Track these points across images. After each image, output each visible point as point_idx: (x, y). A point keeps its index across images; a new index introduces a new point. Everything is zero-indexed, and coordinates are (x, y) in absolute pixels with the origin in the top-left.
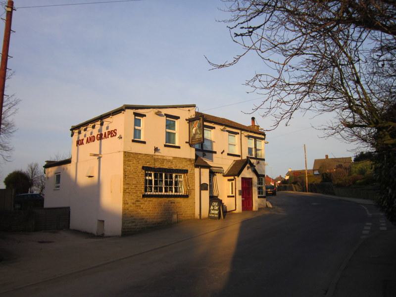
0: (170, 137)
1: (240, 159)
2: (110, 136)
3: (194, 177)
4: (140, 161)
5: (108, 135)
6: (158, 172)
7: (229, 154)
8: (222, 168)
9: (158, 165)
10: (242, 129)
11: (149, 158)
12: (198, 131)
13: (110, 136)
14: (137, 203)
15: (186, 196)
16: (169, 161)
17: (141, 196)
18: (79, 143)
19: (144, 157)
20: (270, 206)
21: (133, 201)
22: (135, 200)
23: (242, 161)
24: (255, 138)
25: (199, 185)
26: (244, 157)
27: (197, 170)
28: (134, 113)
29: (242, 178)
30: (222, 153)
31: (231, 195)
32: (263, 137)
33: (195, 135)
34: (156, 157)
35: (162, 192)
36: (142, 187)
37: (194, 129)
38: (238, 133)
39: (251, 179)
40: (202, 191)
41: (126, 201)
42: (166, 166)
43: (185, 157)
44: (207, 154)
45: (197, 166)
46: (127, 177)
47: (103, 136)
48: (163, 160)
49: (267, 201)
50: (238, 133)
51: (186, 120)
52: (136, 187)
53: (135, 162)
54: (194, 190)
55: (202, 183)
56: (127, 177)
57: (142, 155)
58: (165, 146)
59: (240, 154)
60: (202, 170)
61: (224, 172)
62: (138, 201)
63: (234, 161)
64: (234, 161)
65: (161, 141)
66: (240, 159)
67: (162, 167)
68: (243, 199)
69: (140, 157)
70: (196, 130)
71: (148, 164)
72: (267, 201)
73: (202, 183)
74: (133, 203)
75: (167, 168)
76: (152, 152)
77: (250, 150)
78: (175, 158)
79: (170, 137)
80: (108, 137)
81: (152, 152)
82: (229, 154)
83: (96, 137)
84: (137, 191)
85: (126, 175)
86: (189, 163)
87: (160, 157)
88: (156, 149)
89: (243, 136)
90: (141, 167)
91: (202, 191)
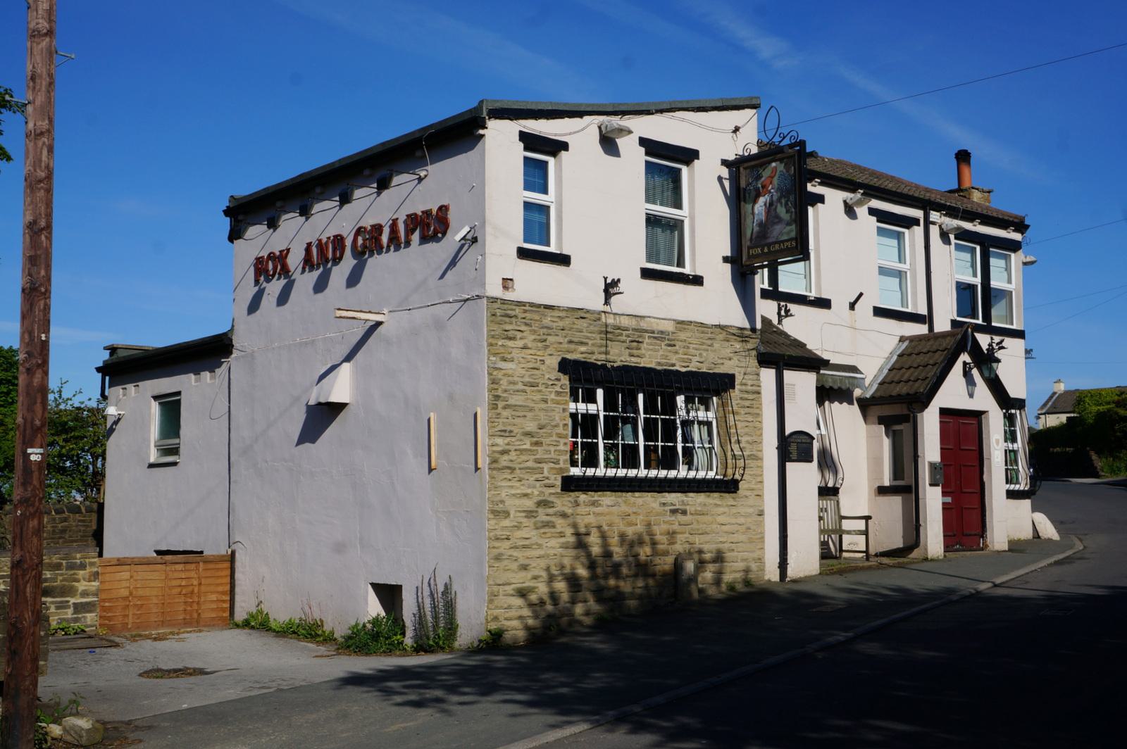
0: (664, 232)
1: (922, 329)
2: (416, 237)
3: (760, 408)
4: (551, 339)
5: (410, 231)
6: (622, 383)
7: (880, 312)
8: (854, 369)
9: (619, 356)
10: (927, 205)
11: (582, 324)
12: (781, 211)
13: (416, 237)
14: (540, 510)
15: (728, 486)
16: (660, 336)
17: (559, 483)
18: (270, 267)
19: (566, 323)
20: (1048, 530)
21: (529, 504)
22: (536, 499)
23: (932, 336)
24: (987, 244)
25: (775, 443)
26: (942, 324)
27: (768, 375)
28: (525, 137)
29: (944, 412)
30: (852, 306)
31: (187, 384)
32: (1017, 236)
33: (764, 227)
34: (611, 320)
35: (595, 465)
36: (562, 447)
37: (762, 200)
38: (916, 222)
39: (978, 415)
40: (789, 465)
41: (502, 502)
42: (651, 358)
43: (723, 323)
44: (793, 307)
45: (765, 360)
46: (501, 404)
47: (385, 238)
48: (638, 334)
49: (1035, 509)
50: (916, 222)
51: (443, 209)
52: (537, 444)
53: (529, 339)
54: (757, 458)
55: (788, 431)
56: (501, 404)
57: (556, 313)
58: (647, 274)
59: (923, 310)
60: (789, 375)
61: (867, 382)
62: (543, 503)
63: (902, 339)
64: (902, 339)
65: (630, 252)
66: (922, 329)
67: (633, 362)
68: (949, 500)
69: (547, 321)
70: (770, 207)
71: (583, 349)
72: (1034, 510)
73: (788, 431)
74: (530, 514)
75: (652, 365)
76: (595, 301)
77: (965, 291)
78: (681, 324)
79: (664, 232)
80: (408, 244)
81: (595, 301)
82: (880, 312)
83: (348, 243)
84: (539, 461)
85: (497, 397)
86: (738, 346)
87: (625, 322)
88: (610, 288)
89: (934, 232)
90: (554, 362)
91: (789, 465)
